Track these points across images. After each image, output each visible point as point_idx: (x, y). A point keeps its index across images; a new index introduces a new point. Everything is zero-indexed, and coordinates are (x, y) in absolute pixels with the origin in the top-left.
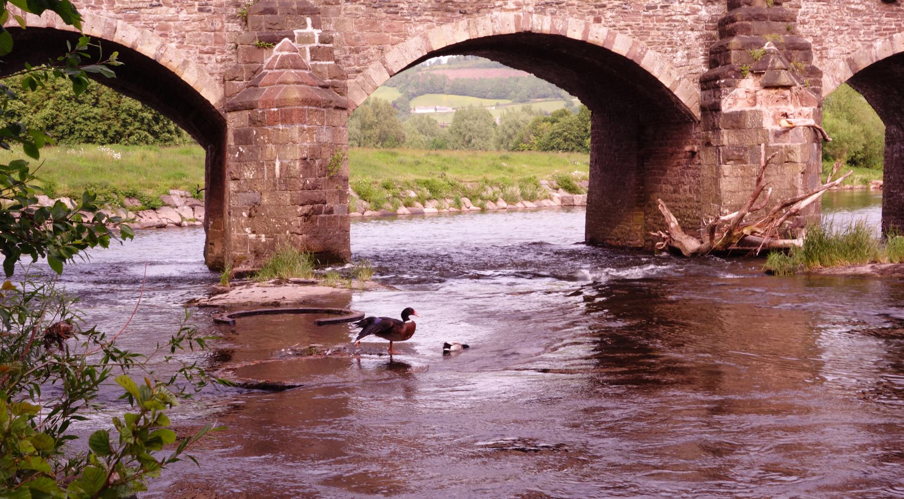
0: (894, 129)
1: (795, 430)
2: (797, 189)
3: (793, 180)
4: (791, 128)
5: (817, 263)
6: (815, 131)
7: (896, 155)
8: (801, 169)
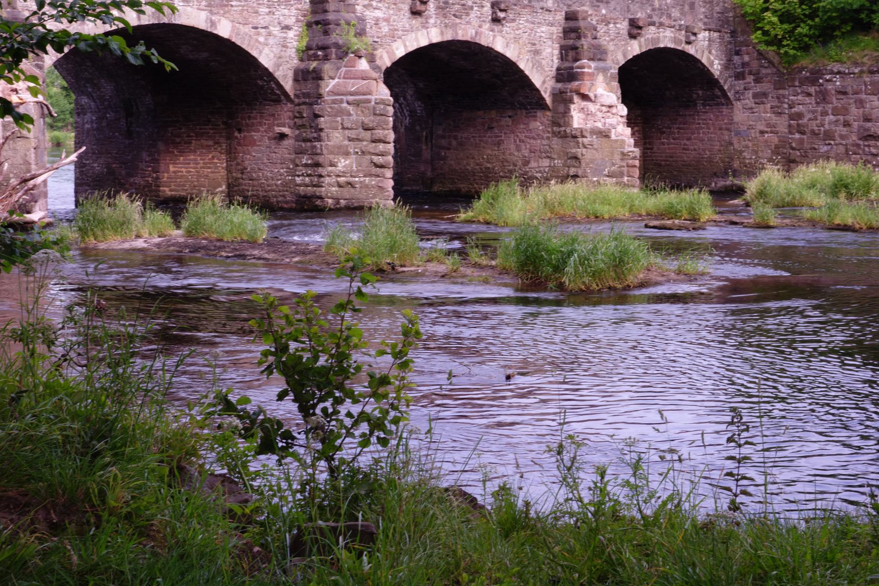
0: (85, 100)
1: (507, 436)
2: (30, 164)
3: (26, 155)
4: (22, 104)
5: (92, 238)
6: (42, 107)
7: (87, 126)
8: (34, 145)
